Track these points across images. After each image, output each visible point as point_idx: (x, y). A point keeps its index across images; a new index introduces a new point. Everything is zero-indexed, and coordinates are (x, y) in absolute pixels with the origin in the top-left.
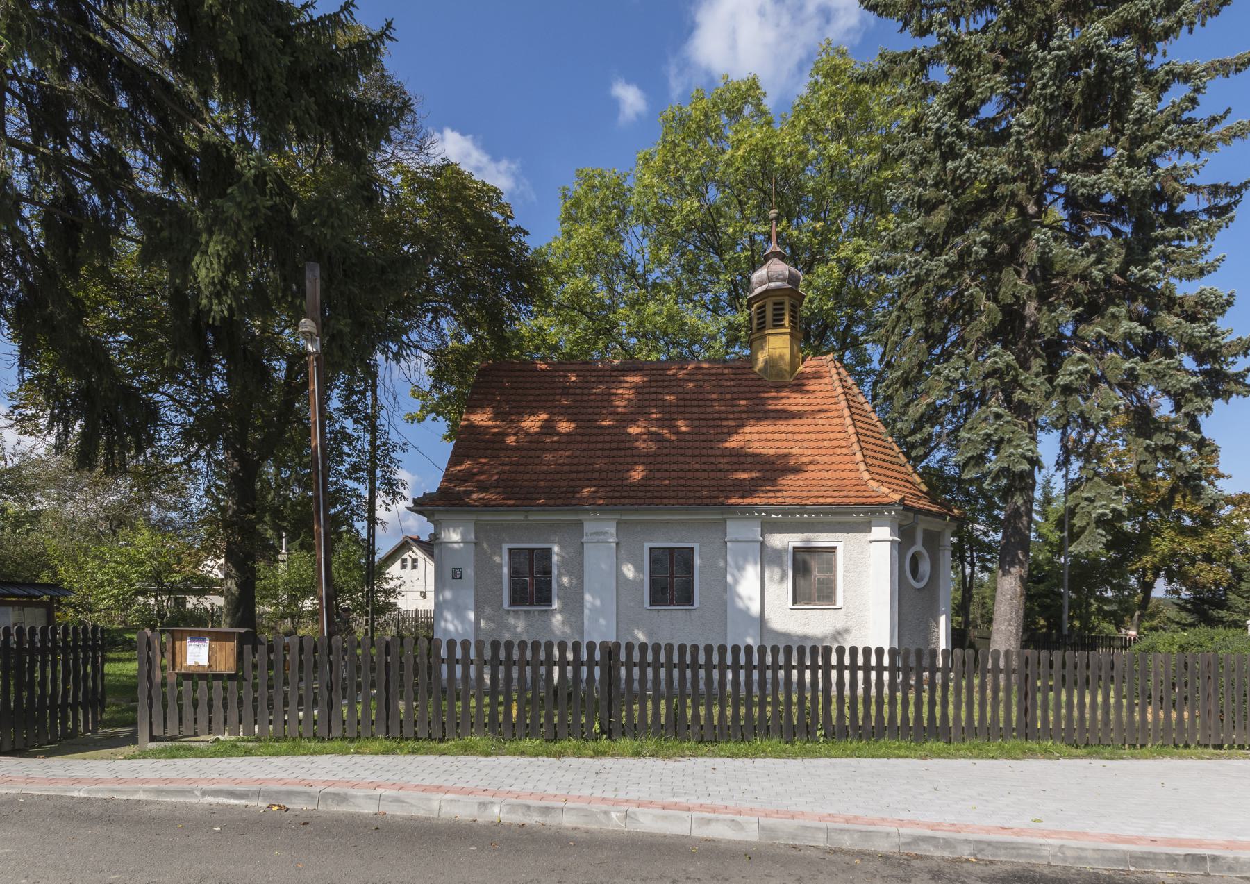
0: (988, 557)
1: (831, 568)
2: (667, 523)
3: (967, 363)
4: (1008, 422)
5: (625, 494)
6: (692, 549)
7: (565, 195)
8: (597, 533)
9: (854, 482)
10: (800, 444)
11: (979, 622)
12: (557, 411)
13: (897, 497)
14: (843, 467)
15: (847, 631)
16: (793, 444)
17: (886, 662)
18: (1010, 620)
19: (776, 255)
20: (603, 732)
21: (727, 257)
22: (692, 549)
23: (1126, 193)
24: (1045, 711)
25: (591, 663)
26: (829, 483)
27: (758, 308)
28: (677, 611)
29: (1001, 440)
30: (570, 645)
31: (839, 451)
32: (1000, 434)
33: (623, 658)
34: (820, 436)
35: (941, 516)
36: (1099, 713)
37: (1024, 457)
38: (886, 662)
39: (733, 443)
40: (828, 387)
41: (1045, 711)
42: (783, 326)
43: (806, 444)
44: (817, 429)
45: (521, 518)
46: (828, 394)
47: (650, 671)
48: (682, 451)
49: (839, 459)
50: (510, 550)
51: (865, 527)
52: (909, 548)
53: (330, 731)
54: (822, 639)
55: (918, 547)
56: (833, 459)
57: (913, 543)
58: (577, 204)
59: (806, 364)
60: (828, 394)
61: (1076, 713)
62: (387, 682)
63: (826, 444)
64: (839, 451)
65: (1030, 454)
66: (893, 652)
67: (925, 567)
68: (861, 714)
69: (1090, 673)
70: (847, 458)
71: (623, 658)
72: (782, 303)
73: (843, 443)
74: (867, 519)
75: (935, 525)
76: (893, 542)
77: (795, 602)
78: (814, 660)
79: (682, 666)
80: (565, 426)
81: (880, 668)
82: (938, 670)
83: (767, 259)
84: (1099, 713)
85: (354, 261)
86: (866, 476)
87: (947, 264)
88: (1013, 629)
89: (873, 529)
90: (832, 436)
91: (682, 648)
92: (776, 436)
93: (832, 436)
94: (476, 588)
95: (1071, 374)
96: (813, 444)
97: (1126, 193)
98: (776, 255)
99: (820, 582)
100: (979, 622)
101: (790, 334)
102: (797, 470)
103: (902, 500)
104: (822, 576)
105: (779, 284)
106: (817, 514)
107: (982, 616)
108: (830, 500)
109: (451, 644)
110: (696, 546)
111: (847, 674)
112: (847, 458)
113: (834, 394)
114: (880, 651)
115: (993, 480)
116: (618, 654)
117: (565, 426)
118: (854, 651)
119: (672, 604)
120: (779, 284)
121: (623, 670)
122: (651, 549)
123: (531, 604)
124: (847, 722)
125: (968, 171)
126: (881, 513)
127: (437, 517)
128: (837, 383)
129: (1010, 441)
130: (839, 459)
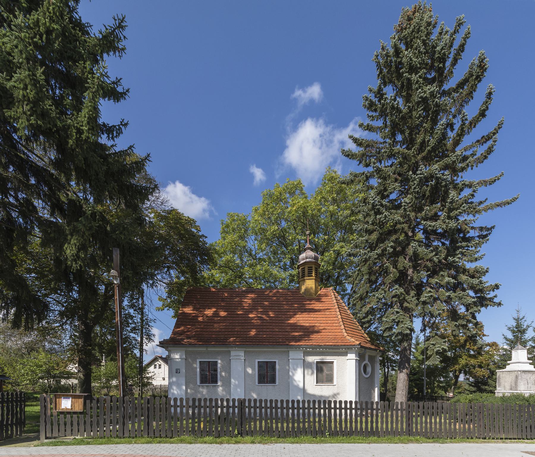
1: (332, 370)
2: (265, 352)
4: (401, 315)
5: (247, 340)
7: (222, 223)
8: (236, 356)
10: (319, 322)
13: (358, 343)
15: (338, 394)
19: (309, 248)
20: (239, 434)
23: (447, 229)
25: (234, 407)
26: (331, 337)
27: (302, 269)
29: (399, 321)
31: (335, 325)
33: (247, 404)
34: (327, 319)
39: (292, 321)
40: (330, 300)
42: (312, 276)
43: (321, 322)
44: (326, 316)
46: (330, 303)
49: (334, 328)
50: (200, 362)
51: (345, 354)
52: (363, 362)
53: (124, 434)
54: (328, 397)
55: (366, 362)
56: (332, 328)
57: (365, 360)
58: (227, 226)
59: (321, 291)
60: (330, 303)
64: (335, 325)
65: (410, 327)
66: (356, 403)
67: (369, 369)
69: (434, 411)
71: (247, 404)
72: (312, 267)
73: (336, 322)
74: (346, 351)
75: (373, 353)
76: (356, 360)
77: (317, 383)
80: (223, 314)
83: (305, 250)
86: (345, 334)
87: (377, 254)
90: (332, 319)
92: (309, 319)
93: (332, 319)
94: (186, 377)
95: (426, 297)
96: (325, 322)
97: (447, 229)
98: (309, 248)
101: (315, 279)
102: (318, 332)
103: (360, 344)
104: (328, 373)
105: (310, 260)
108: (331, 344)
110: (277, 361)
113: (333, 302)
114: (351, 402)
115: (396, 337)
116: (245, 403)
117: (223, 314)
118: (340, 402)
119: (267, 383)
120: (310, 260)
123: (209, 383)
125: (385, 219)
126: (352, 349)
127: (169, 349)
128: (334, 299)
129: (402, 322)
130: (334, 328)
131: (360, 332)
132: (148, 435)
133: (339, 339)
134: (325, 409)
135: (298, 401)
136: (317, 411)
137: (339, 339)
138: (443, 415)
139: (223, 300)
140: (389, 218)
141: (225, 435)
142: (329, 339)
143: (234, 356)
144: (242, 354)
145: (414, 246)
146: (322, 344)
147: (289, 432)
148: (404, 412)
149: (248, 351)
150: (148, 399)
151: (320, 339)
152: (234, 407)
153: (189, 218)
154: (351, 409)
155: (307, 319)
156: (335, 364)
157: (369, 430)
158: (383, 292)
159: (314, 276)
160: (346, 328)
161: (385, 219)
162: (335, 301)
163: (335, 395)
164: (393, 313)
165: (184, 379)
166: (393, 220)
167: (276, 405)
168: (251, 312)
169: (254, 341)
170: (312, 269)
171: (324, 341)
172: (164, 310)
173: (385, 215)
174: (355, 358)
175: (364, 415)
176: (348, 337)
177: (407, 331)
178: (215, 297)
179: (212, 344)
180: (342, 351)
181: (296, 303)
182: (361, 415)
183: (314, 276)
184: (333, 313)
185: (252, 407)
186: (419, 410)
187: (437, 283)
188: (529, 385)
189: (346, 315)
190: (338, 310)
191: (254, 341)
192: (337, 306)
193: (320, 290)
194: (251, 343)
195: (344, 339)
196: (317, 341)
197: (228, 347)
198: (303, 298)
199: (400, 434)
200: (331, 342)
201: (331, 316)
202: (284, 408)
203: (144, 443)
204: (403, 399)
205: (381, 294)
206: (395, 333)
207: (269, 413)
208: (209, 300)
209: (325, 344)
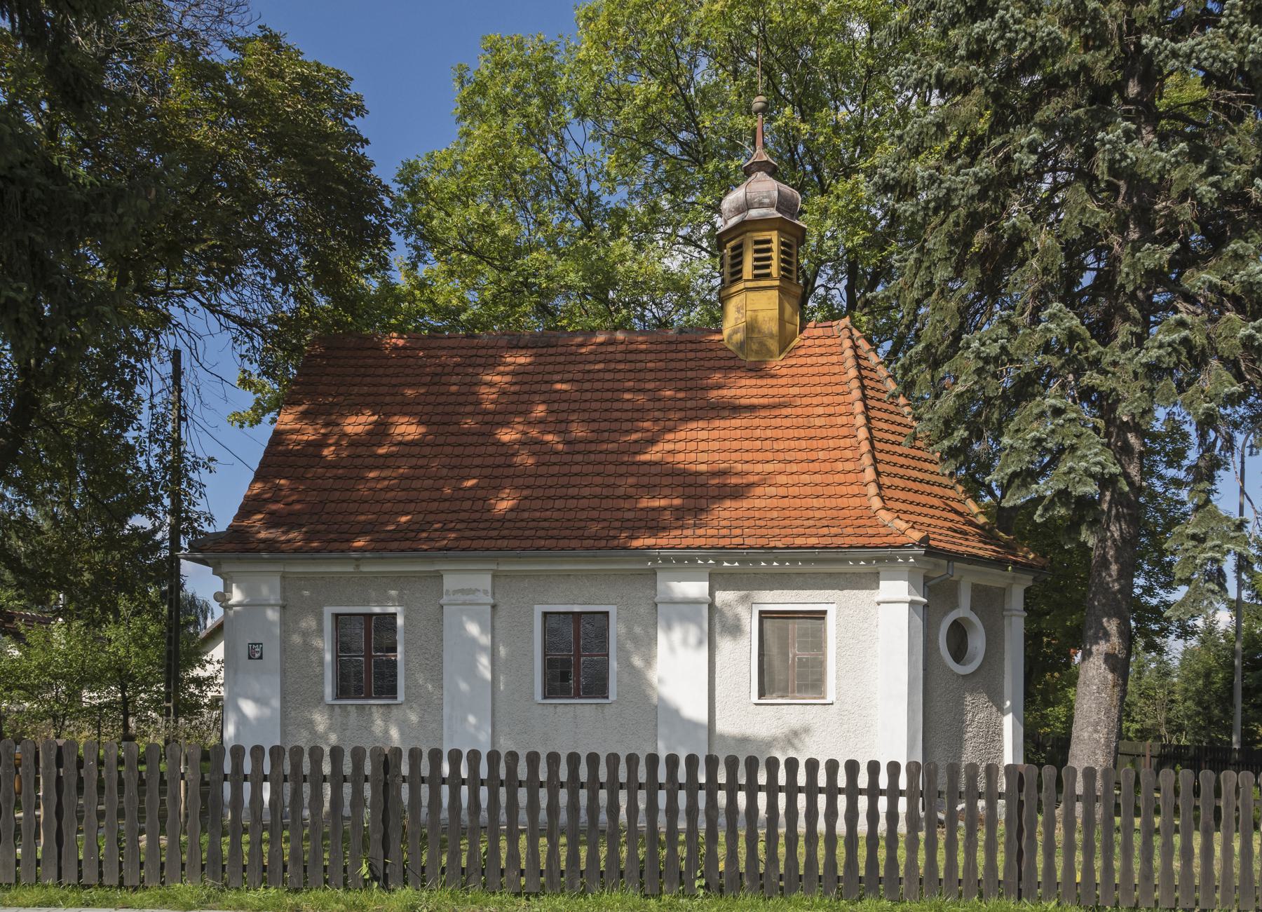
0: (1155, 627)
1: (818, 643)
3: (1014, 329)
4: (1070, 420)
5: (505, 533)
6: (607, 613)
7: (461, 77)
8: (462, 591)
9: (858, 513)
10: (781, 456)
11: (1163, 731)
12: (387, 407)
13: (916, 536)
14: (843, 490)
16: (770, 456)
17: (903, 784)
18: (1097, 724)
19: (762, 166)
20: (374, 878)
21: (711, 167)
22: (607, 613)
23: (1241, 64)
24: (1049, 855)
25: (358, 778)
26: (818, 514)
27: (733, 249)
28: (584, 708)
29: (1061, 450)
30: (327, 750)
31: (840, 466)
32: (1058, 439)
33: (405, 770)
34: (814, 444)
35: (999, 563)
36: (801, 849)
37: (1087, 472)
38: (903, 784)
39: (653, 454)
40: (836, 369)
41: (1049, 855)
42: (768, 276)
43: (789, 456)
44: (812, 432)
45: (350, 569)
46: (834, 379)
47: (543, 794)
48: (600, 468)
49: (839, 478)
50: (336, 616)
51: (870, 581)
52: (946, 614)
53: (80, 877)
54: (770, 744)
55: (963, 611)
56: (830, 478)
57: (955, 605)
58: (481, 89)
59: (806, 333)
60: (834, 379)
63: (821, 455)
64: (840, 466)
65: (1098, 469)
66: (913, 768)
67: (977, 642)
68: (802, 860)
69: (1222, 804)
70: (851, 478)
71: (405, 770)
72: (769, 241)
73: (848, 454)
74: (869, 569)
75: (994, 578)
76: (912, 604)
77: (762, 694)
79: (574, 784)
80: (407, 429)
81: (893, 793)
82: (1097, 799)
83: (748, 172)
84: (801, 849)
85: (38, 194)
86: (876, 503)
87: (978, 181)
88: (1101, 737)
90: (832, 443)
91: (832, 766)
92: (747, 445)
93: (832, 443)
94: (284, 672)
95: (1161, 346)
96: (803, 456)
97: (1241, 64)
98: (762, 166)
99: (802, 663)
100: (1163, 731)
101: (780, 289)
102: (738, 493)
103: (925, 540)
104: (805, 655)
105: (763, 211)
107: (1168, 721)
108: (812, 541)
110: (612, 609)
111: (802, 800)
112: (851, 478)
113: (844, 378)
114: (894, 768)
115: (1046, 509)
116: (398, 766)
117: (407, 429)
118: (812, 765)
119: (578, 696)
120: (763, 211)
121: (405, 790)
122: (546, 615)
123: (369, 697)
124: (742, 866)
125: (1002, 37)
126: (692, 560)
127: (225, 568)
128: (850, 362)
129: (1073, 448)
130: (839, 478)
131: (950, 493)
132: (60, 877)
133: (848, 522)
134: (772, 789)
135: (474, 756)
136: (722, 797)
137: (848, 522)
138: (1040, 818)
139: (436, 379)
140: (1017, 32)
141: (326, 882)
142: (811, 523)
143: (456, 592)
144: (485, 581)
145: (1110, 142)
146: (779, 544)
147: (557, 874)
148: (1002, 802)
149: (508, 575)
150: (60, 748)
151: (775, 523)
152: (358, 778)
153: (319, 67)
154: (893, 793)
155: (736, 445)
156: (831, 619)
157: (801, 872)
158: (1003, 331)
159: (775, 274)
160: (885, 480)
161: (1002, 37)
162: (853, 373)
163: (793, 737)
164: (1042, 414)
165: (277, 680)
166: (1033, 37)
167: (512, 771)
168: (507, 424)
169: (527, 533)
170: (769, 250)
171: (788, 531)
172: (259, 421)
173: (1002, 18)
174: (909, 598)
175: (941, 822)
176: (882, 513)
177: (1085, 484)
178: (408, 371)
179: (356, 550)
180: (856, 569)
182: (933, 824)
183: (775, 274)
184: (843, 420)
186: (1062, 797)
187: (1212, 287)
189: (893, 428)
190: (859, 407)
191: (527, 533)
192: (856, 394)
193: (801, 332)
194: (516, 543)
195: (868, 522)
196: (763, 531)
197: (432, 560)
198: (732, 363)
200: (816, 535)
201: (831, 432)
202: (541, 785)
203: (27, 906)
204: (1096, 761)
205: (995, 341)
206: (1042, 498)
207: (484, 803)
208: (385, 380)
209: (788, 541)
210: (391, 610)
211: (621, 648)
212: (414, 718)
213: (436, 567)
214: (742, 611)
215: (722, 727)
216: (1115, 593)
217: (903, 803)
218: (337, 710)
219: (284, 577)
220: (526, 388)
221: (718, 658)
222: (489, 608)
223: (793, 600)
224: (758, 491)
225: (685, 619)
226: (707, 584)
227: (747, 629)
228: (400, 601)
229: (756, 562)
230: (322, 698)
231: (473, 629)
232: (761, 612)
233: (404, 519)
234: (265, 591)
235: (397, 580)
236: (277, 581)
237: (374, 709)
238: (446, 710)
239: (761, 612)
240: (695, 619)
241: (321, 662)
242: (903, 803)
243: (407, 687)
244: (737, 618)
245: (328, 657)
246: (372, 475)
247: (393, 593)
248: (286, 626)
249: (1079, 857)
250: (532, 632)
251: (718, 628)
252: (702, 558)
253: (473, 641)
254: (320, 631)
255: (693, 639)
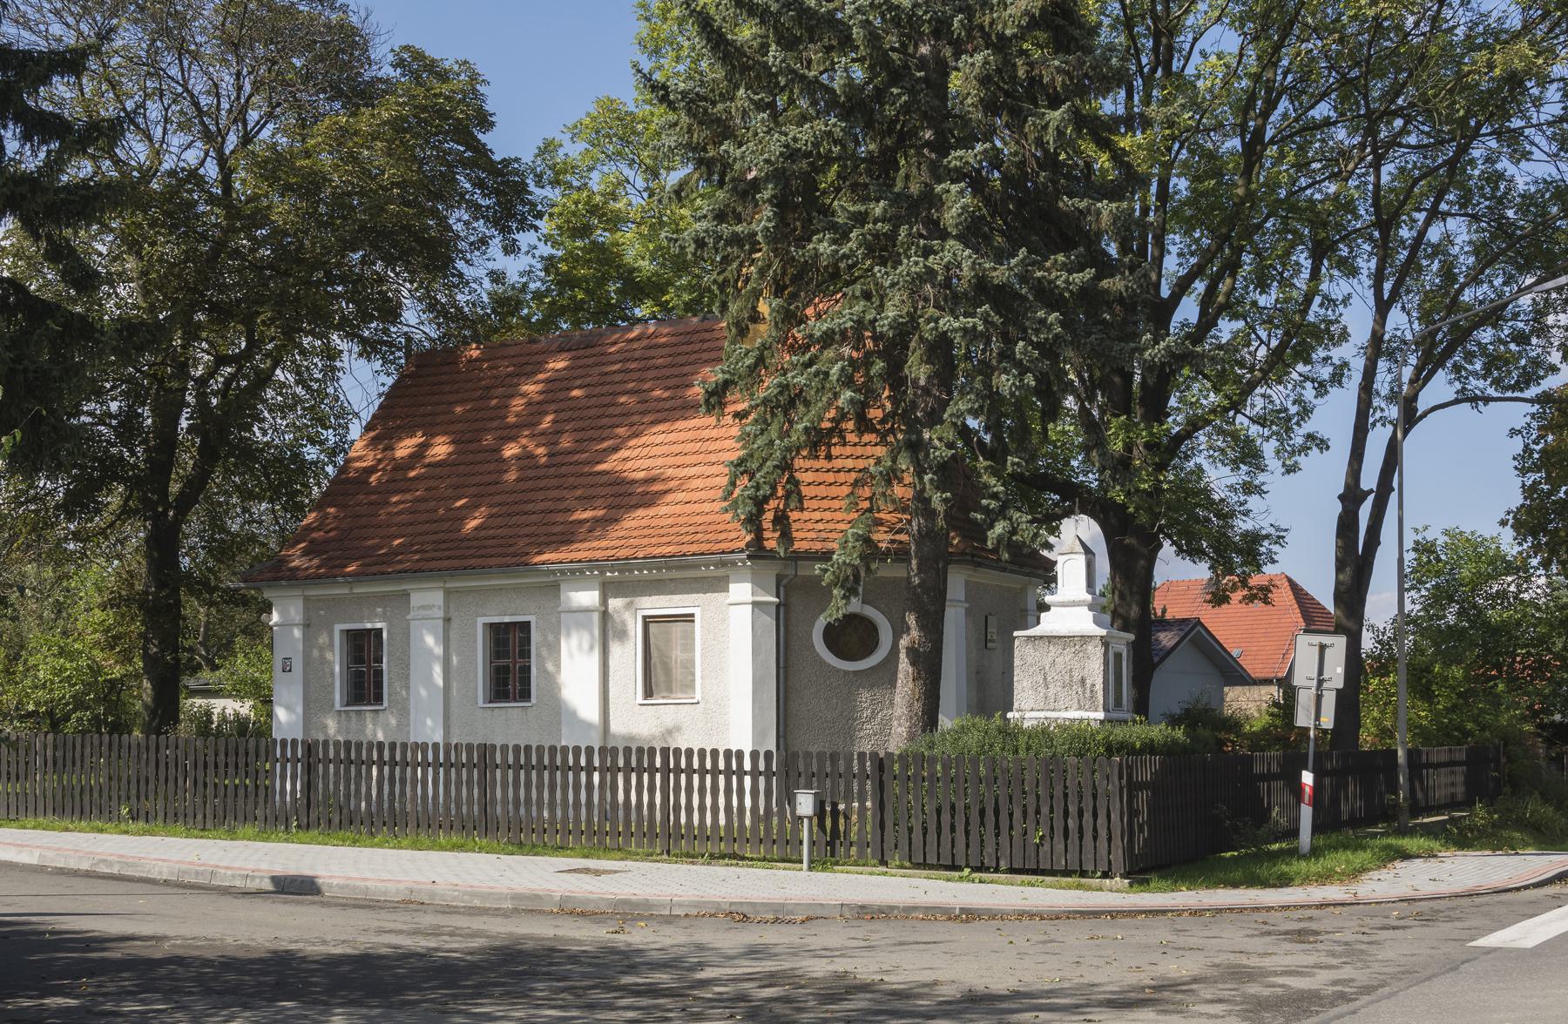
2: (500, 589)
15: (678, 729)
51: (718, 584)
61: (559, 813)
62: (1095, 807)
76: (755, 604)
77: (649, 692)
78: (640, 760)
89: (731, 586)
94: (306, 685)
102: (649, 500)
106: (659, 569)
109: (284, 742)
110: (697, 612)
114: (294, 742)
126: (582, 572)
135: (590, 750)
143: (419, 608)
149: (458, 591)
156: (697, 619)
174: (750, 599)
181: (578, 382)
185: (720, 772)
188: (1052, 691)
194: (456, 563)
199: (1067, 873)
210: (379, 625)
211: (538, 655)
212: (393, 721)
213: (403, 587)
214: (627, 616)
215: (616, 727)
216: (915, 587)
217: (596, 777)
218: (343, 715)
219: (306, 599)
220: (676, 371)
221: (612, 663)
222: (441, 622)
223: (667, 605)
224: (669, 498)
225: (581, 626)
226: (597, 593)
227: (632, 633)
228: (384, 618)
229: (631, 571)
230: (333, 705)
231: (430, 640)
232: (645, 617)
233: (397, 542)
234: (292, 611)
235: (383, 598)
236: (300, 603)
237: (368, 714)
238: (412, 712)
239: (645, 617)
240: (586, 626)
241: (332, 674)
242: (596, 777)
243: (390, 695)
244: (624, 623)
245: (337, 669)
246: (394, 499)
247: (379, 610)
248: (308, 640)
249: (534, 796)
250: (475, 641)
251: (610, 634)
252: (588, 569)
253: (430, 651)
254: (331, 645)
255: (586, 645)
